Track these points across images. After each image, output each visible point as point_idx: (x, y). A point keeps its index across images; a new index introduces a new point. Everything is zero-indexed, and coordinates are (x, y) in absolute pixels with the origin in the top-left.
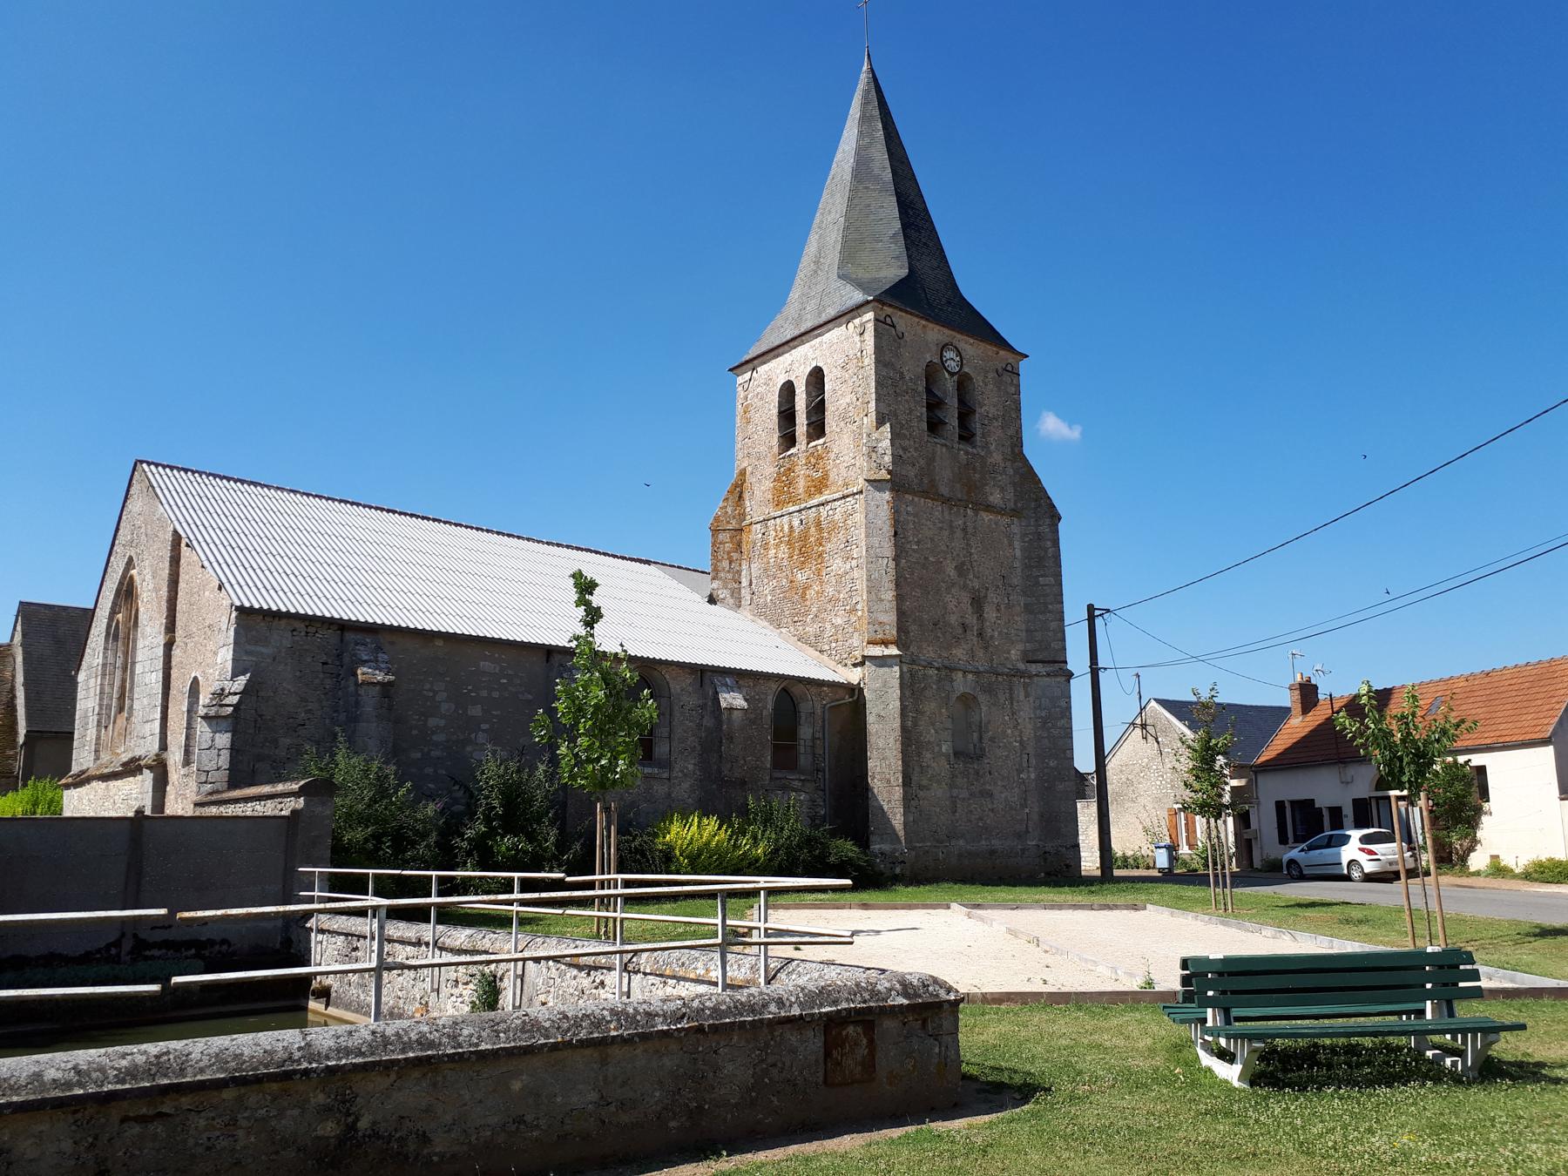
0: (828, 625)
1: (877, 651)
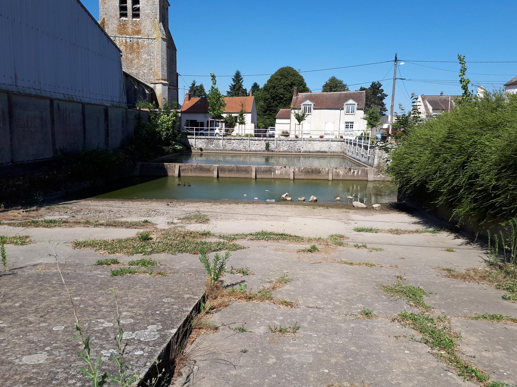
0: (141, 72)
1: (164, 82)
